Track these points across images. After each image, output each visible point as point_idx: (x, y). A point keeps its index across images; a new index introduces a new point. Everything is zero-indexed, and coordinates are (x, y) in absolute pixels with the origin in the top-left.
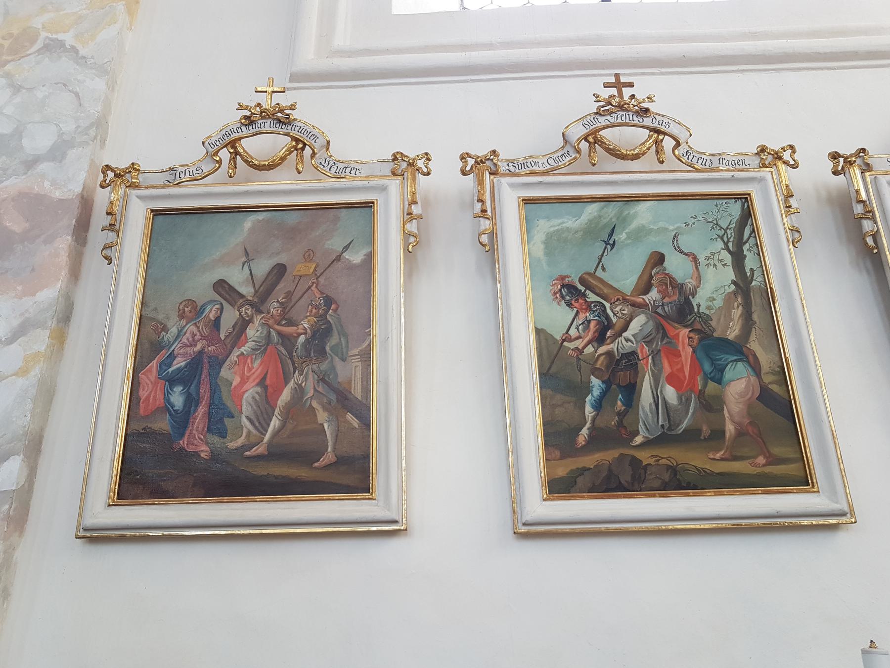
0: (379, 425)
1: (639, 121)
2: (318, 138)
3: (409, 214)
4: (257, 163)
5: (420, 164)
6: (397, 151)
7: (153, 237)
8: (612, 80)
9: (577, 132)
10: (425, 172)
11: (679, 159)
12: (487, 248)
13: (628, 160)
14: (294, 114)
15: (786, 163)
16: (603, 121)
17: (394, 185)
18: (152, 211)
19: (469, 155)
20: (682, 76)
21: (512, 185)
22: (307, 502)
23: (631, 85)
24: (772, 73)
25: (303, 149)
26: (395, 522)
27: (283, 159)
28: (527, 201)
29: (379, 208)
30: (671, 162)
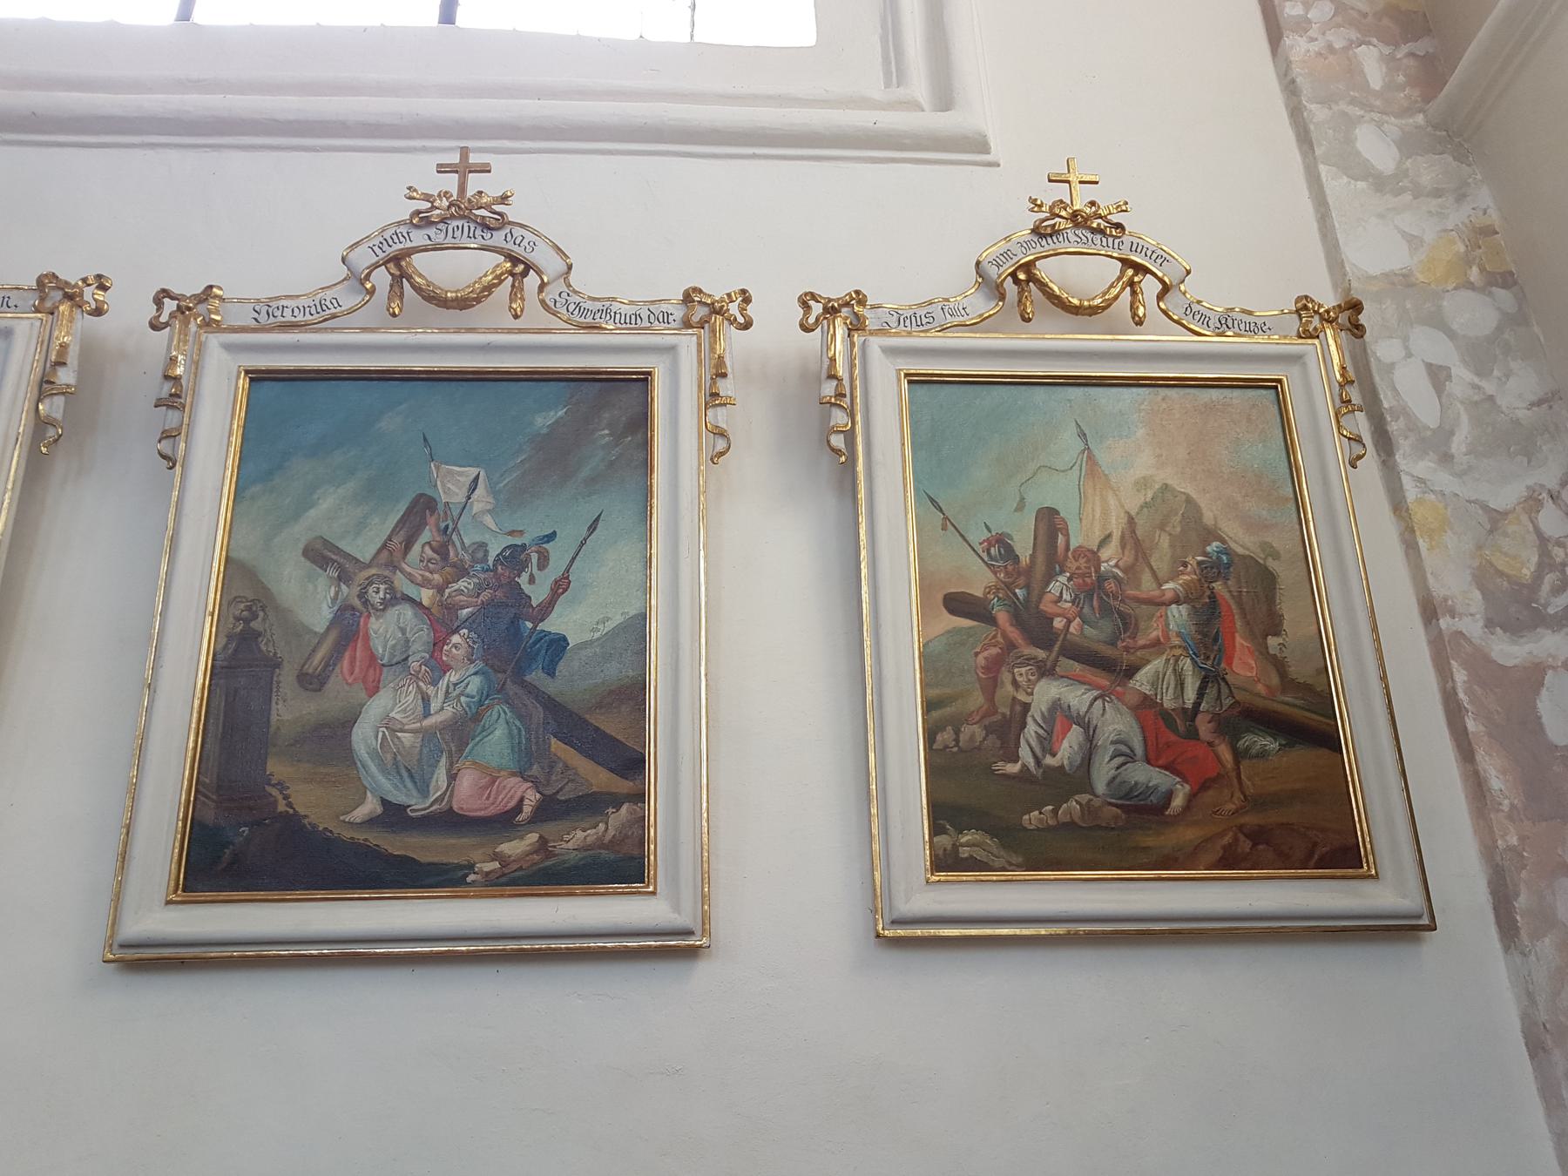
0: (697, 721)
1: (483, 237)
3: (715, 395)
4: (1076, 302)
5: (734, 309)
6: (692, 285)
8: (455, 158)
9: (363, 258)
10: (741, 324)
12: (843, 459)
13: (1083, 315)
14: (511, 212)
15: (732, 321)
16: (419, 238)
17: (687, 343)
18: (247, 372)
19: (813, 296)
20: (44, 150)
21: (228, 347)
23: (485, 169)
24: (206, 152)
25: (525, 274)
27: (489, 288)
28: (915, 381)
30: (534, 314)
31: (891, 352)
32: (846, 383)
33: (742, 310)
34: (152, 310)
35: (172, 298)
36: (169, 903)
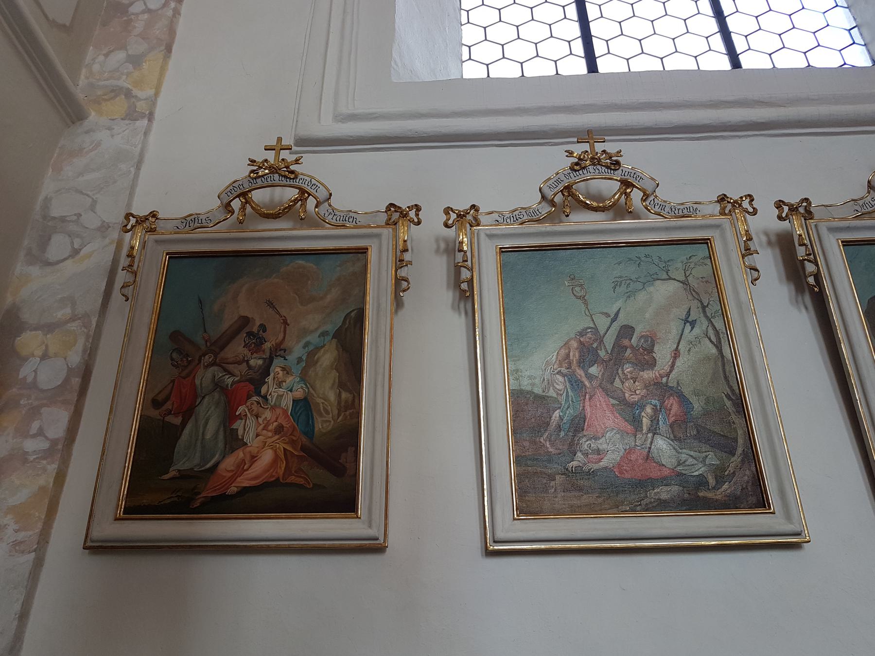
2: (319, 187)
3: (401, 261)
7: (504, 268)
11: (323, 221)
15: (412, 221)
17: (387, 232)
19: (452, 210)
22: (720, 516)
26: (798, 534)
29: (372, 255)
31: (491, 236)
32: (809, 246)
33: (417, 215)
34: (776, 212)
35: (134, 217)
36: (116, 519)
